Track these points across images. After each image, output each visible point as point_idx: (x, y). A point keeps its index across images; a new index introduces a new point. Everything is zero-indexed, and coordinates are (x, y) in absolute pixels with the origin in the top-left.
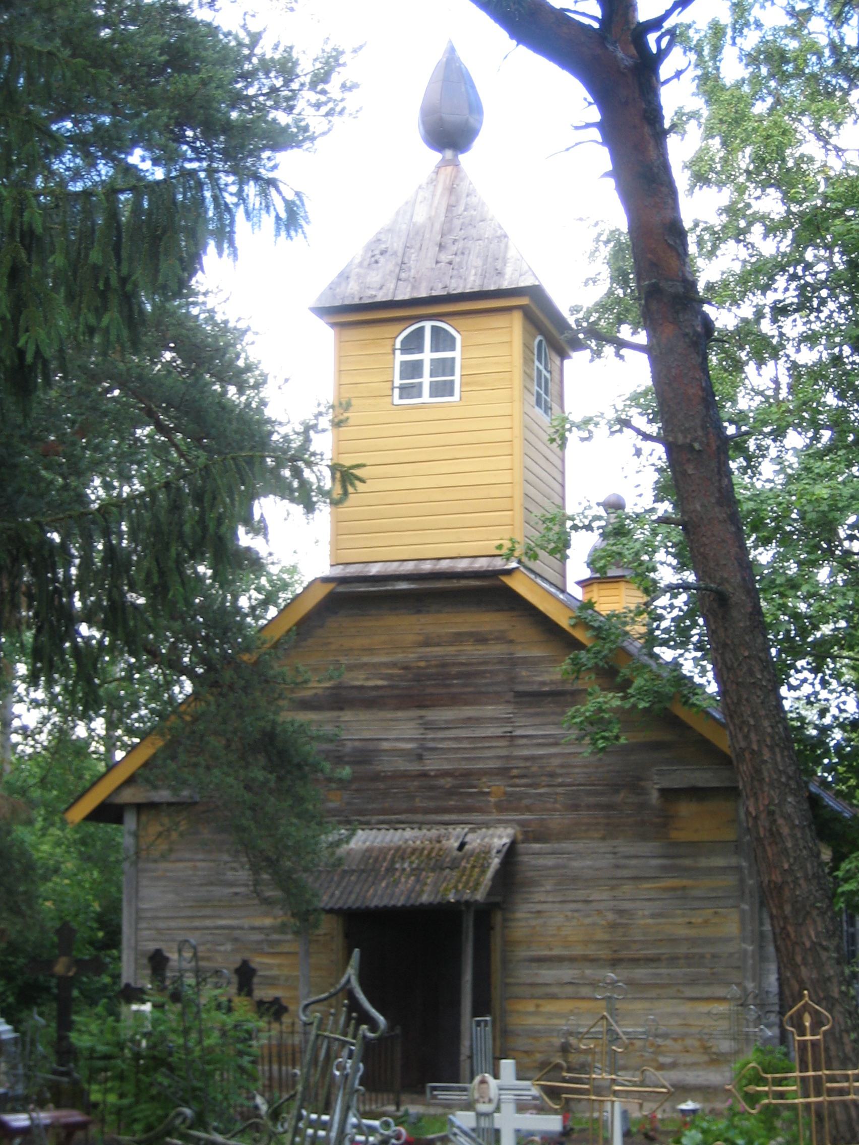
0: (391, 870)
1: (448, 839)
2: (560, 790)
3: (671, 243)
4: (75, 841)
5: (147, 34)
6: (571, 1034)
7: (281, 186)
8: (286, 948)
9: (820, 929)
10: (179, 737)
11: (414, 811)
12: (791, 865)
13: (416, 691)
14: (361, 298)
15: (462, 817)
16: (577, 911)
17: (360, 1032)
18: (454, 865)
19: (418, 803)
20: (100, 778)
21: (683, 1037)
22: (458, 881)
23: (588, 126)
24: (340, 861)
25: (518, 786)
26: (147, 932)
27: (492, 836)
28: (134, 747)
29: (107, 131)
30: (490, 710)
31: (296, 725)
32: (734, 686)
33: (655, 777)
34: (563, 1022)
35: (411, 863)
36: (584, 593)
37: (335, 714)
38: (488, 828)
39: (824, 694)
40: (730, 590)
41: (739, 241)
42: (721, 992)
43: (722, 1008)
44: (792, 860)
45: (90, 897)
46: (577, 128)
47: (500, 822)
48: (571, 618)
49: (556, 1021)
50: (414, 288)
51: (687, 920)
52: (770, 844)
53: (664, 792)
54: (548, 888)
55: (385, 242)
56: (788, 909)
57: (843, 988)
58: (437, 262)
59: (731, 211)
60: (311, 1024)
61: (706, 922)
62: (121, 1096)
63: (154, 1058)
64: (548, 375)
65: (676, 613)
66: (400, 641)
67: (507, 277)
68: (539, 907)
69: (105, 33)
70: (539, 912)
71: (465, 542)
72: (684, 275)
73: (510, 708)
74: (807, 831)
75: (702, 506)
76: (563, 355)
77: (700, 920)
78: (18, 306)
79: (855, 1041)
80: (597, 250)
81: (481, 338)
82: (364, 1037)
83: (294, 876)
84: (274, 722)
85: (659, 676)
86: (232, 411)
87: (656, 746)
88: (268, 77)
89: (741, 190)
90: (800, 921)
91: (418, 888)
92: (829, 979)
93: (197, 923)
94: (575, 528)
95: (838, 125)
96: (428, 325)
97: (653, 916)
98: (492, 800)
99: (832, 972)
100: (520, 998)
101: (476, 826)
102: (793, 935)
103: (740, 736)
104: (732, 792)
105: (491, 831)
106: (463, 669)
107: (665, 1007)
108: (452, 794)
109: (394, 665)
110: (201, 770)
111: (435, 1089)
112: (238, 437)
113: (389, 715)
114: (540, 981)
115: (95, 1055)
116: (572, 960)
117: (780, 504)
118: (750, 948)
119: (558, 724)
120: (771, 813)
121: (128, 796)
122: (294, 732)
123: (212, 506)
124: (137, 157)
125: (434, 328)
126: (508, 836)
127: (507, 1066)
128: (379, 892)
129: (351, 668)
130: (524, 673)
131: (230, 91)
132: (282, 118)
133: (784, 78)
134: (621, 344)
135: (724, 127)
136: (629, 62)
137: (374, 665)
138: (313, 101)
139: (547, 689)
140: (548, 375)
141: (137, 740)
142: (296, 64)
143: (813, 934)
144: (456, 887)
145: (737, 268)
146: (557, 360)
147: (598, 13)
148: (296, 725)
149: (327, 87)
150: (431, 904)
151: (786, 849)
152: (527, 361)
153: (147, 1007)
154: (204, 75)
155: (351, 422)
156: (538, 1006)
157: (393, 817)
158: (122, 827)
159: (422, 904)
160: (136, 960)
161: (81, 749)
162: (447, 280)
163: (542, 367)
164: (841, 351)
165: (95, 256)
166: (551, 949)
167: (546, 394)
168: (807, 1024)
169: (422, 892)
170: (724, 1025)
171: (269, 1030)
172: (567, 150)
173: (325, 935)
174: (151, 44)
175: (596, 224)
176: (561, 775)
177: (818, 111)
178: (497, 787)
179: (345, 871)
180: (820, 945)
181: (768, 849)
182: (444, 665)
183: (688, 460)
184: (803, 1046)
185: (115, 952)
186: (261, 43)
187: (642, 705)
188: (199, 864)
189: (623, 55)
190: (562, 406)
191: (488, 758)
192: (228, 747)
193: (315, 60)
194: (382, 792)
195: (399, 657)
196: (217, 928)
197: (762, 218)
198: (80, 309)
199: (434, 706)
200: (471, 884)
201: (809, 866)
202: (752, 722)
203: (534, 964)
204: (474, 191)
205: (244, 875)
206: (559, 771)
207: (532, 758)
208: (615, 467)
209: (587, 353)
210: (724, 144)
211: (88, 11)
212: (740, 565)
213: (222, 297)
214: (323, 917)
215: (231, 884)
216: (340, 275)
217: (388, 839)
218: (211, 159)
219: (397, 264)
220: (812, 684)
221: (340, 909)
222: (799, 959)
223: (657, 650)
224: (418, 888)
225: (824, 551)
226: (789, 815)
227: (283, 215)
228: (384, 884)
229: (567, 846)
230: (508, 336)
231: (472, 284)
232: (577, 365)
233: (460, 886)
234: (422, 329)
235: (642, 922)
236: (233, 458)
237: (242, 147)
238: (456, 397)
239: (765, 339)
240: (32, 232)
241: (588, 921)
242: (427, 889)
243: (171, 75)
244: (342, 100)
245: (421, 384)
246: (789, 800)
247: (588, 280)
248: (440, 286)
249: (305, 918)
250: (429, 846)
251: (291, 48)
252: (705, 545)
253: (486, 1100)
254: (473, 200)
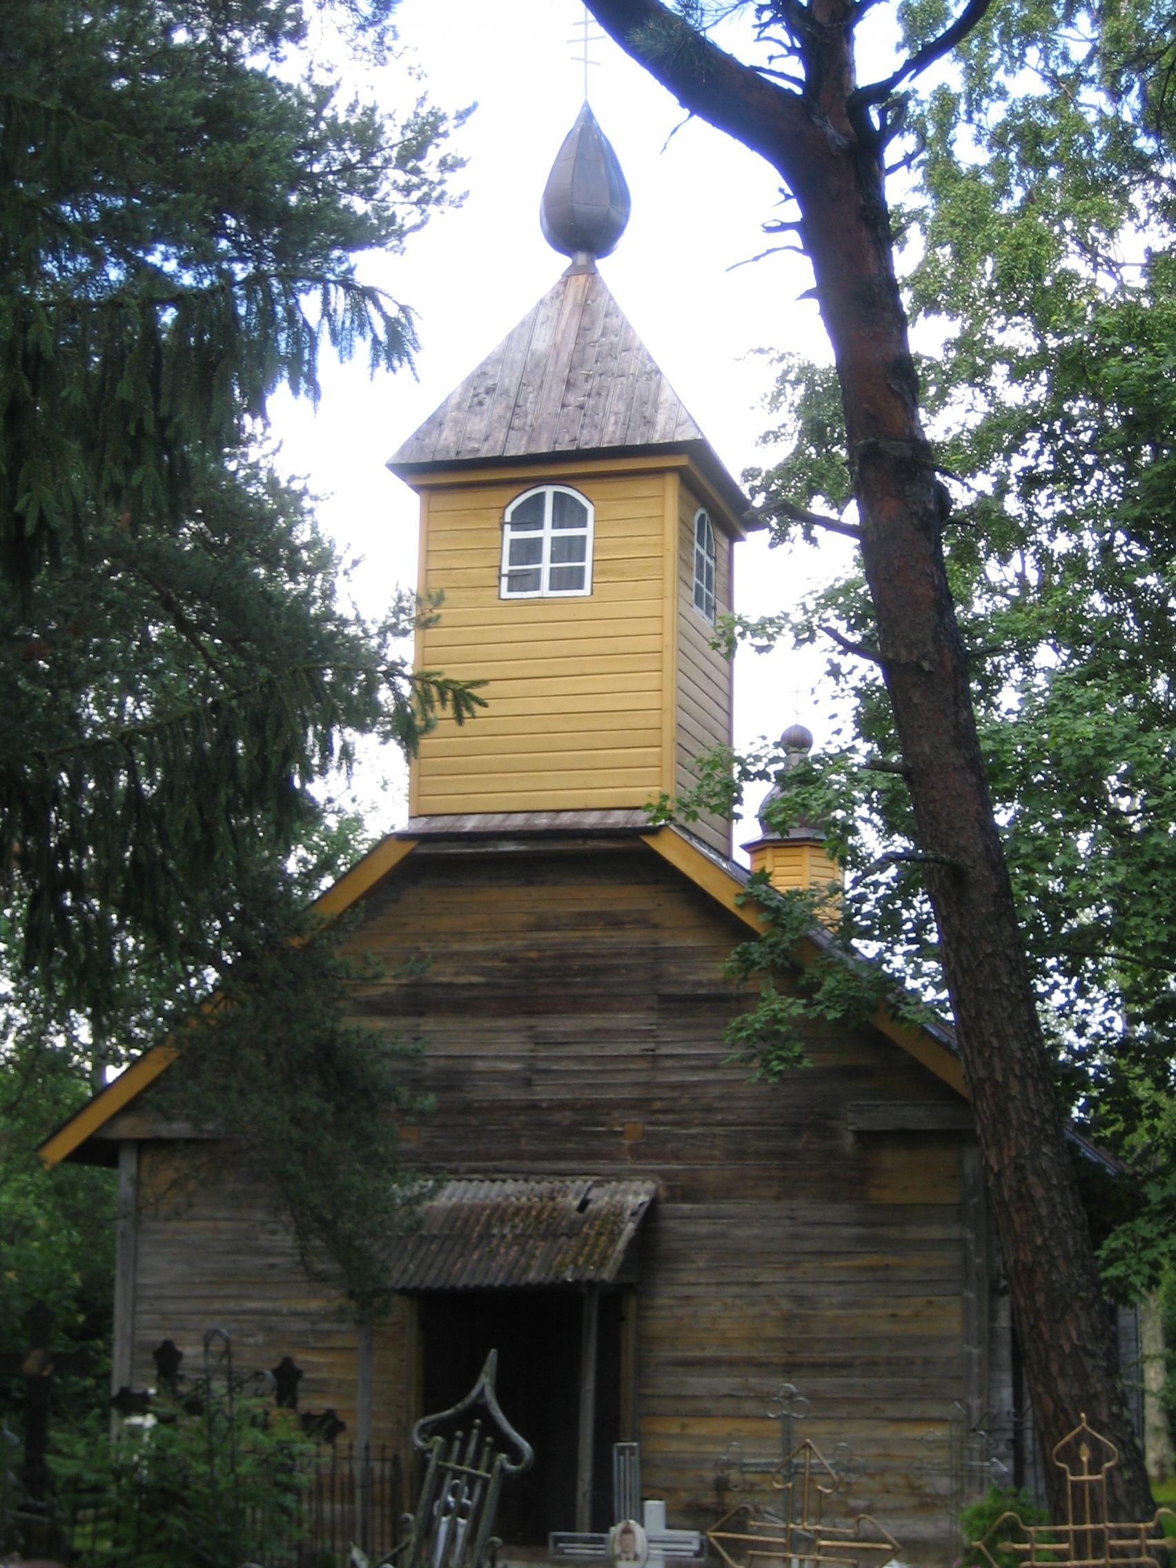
0: (486, 1236)
1: (565, 1195)
2: (718, 1130)
3: (896, 388)
4: (47, 1191)
5: (179, 88)
6: (729, 1465)
7: (383, 300)
8: (338, 1342)
9: (1083, 1328)
10: (198, 1053)
11: (518, 1156)
12: (1045, 1239)
13: (524, 991)
14: (458, 453)
15: (584, 1166)
16: (739, 1296)
17: (498, 1463)
18: (573, 1231)
19: (524, 1145)
20: (87, 1104)
21: (882, 1472)
22: (579, 1254)
23: (784, 227)
24: (420, 1222)
25: (662, 1124)
26: (147, 1317)
27: (625, 1192)
28: (135, 1061)
29: (121, 218)
30: (624, 1020)
31: (363, 1036)
32: (972, 995)
33: (850, 1115)
34: (720, 1449)
35: (514, 1227)
36: (753, 862)
37: (412, 1021)
38: (619, 1181)
39: (1081, 1005)
40: (969, 863)
41: (972, 384)
42: (937, 1411)
43: (939, 1432)
44: (1047, 1233)
45: (68, 1267)
46: (770, 230)
47: (636, 1173)
48: (738, 895)
49: (709, 1448)
50: (531, 440)
51: (890, 1311)
52: (1018, 1211)
53: (860, 1135)
54: (701, 1264)
55: (492, 377)
56: (1040, 1299)
57: (1115, 1409)
58: (563, 406)
59: (964, 344)
60: (430, 1451)
61: (916, 1314)
62: (117, 1543)
63: (163, 1491)
64: (712, 563)
65: (882, 891)
66: (502, 922)
67: (659, 427)
68: (689, 1291)
69: (121, 83)
70: (687, 1297)
71: (606, 786)
72: (911, 432)
73: (653, 1018)
74: (1069, 1194)
75: (933, 747)
76: (734, 536)
77: (907, 1312)
78: (17, 456)
79: (1130, 1481)
80: (780, 393)
81: (621, 510)
82: (503, 1470)
83: (357, 1243)
84: (333, 1031)
85: (856, 977)
86: (281, 604)
87: (848, 1073)
88: (340, 149)
89: (979, 319)
90: (1057, 1316)
91: (523, 1261)
92: (1095, 1396)
93: (216, 1306)
94: (745, 774)
95: (1111, 233)
96: (549, 491)
97: (844, 1305)
98: (626, 1142)
99: (1099, 1387)
100: (662, 1415)
101: (604, 1179)
102: (1046, 1336)
103: (979, 1062)
104: (958, 1137)
105: (623, 1186)
106: (589, 962)
107: (858, 1430)
108: (574, 1133)
109: (495, 955)
110: (234, 1096)
111: (559, 1540)
112: (289, 640)
113: (487, 1024)
114: (687, 1391)
115: (81, 1486)
116: (731, 1363)
117: (1029, 744)
118: (976, 1351)
119: (719, 1040)
120: (1020, 1168)
121: (126, 1129)
122: (360, 1045)
123: (277, 735)
124: (162, 258)
125: (557, 495)
126: (647, 1193)
127: (655, 1508)
128: (470, 1267)
129: (437, 958)
130: (673, 969)
131: (289, 167)
132: (360, 206)
133: (1041, 164)
134: (810, 521)
135: (957, 232)
136: (841, 142)
137: (466, 955)
138: (401, 183)
139: (703, 991)
140: (712, 563)
141: (138, 1053)
142: (379, 131)
143: (1074, 1334)
144: (574, 1262)
145: (975, 420)
146: (725, 543)
147: (800, 73)
148: (363, 1036)
149: (422, 165)
150: (540, 1284)
151: (1039, 1218)
152: (684, 543)
153: (149, 1421)
154: (252, 143)
155: (443, 621)
156: (684, 1426)
157: (490, 1164)
158: (116, 1171)
159: (527, 1285)
160: (132, 1354)
161: (59, 1062)
162: (576, 430)
163: (703, 552)
164: (1112, 538)
165: (124, 390)
166: (703, 1349)
167: (709, 588)
168: (1084, 1459)
169: (528, 1267)
170: (940, 1456)
171: (318, 1455)
172: (756, 259)
173: (394, 1324)
174: (183, 102)
175: (782, 358)
176: (720, 1110)
177: (1085, 211)
178: (633, 1125)
179: (423, 1238)
180: (1084, 1349)
181: (1015, 1216)
182: (563, 957)
183: (914, 685)
184: (1077, 1486)
185: (100, 1343)
186: (333, 102)
187: (831, 1015)
188: (222, 1224)
189: (835, 132)
190: (730, 606)
191: (624, 1085)
192: (268, 1063)
193: (405, 127)
194: (479, 1129)
195: (502, 944)
196: (244, 1312)
197: (1005, 355)
198: (102, 461)
199: (548, 1012)
200: (596, 1258)
201: (1070, 1241)
202: (995, 1043)
203: (680, 1369)
204: (616, 308)
205: (286, 1240)
206: (717, 1104)
207: (682, 1086)
208: (798, 690)
209: (764, 536)
210: (956, 254)
211: (97, 54)
212: (983, 829)
213: (268, 447)
214: (396, 1299)
215: (266, 1253)
216: (431, 420)
217: (482, 1194)
218: (260, 258)
219: (508, 407)
220: (1066, 992)
221: (416, 1289)
222: (1054, 1369)
223: (855, 942)
224: (523, 1261)
225: (1084, 809)
226: (1044, 1171)
227: (383, 337)
228: (475, 1257)
229: (727, 1207)
230: (658, 511)
231: (611, 435)
232: (752, 549)
233: (581, 1260)
234: (541, 496)
235: (829, 1313)
236: (307, 671)
237: (303, 243)
238: (586, 591)
239: (1009, 523)
240: (38, 355)
241: (754, 1311)
242: (536, 1263)
243: (208, 143)
244: (441, 182)
245: (538, 571)
246: (1045, 1150)
247: (767, 434)
248: (567, 437)
249: (366, 1298)
250: (539, 1205)
251: (373, 110)
252: (934, 801)
253: (631, 1556)
254: (615, 322)
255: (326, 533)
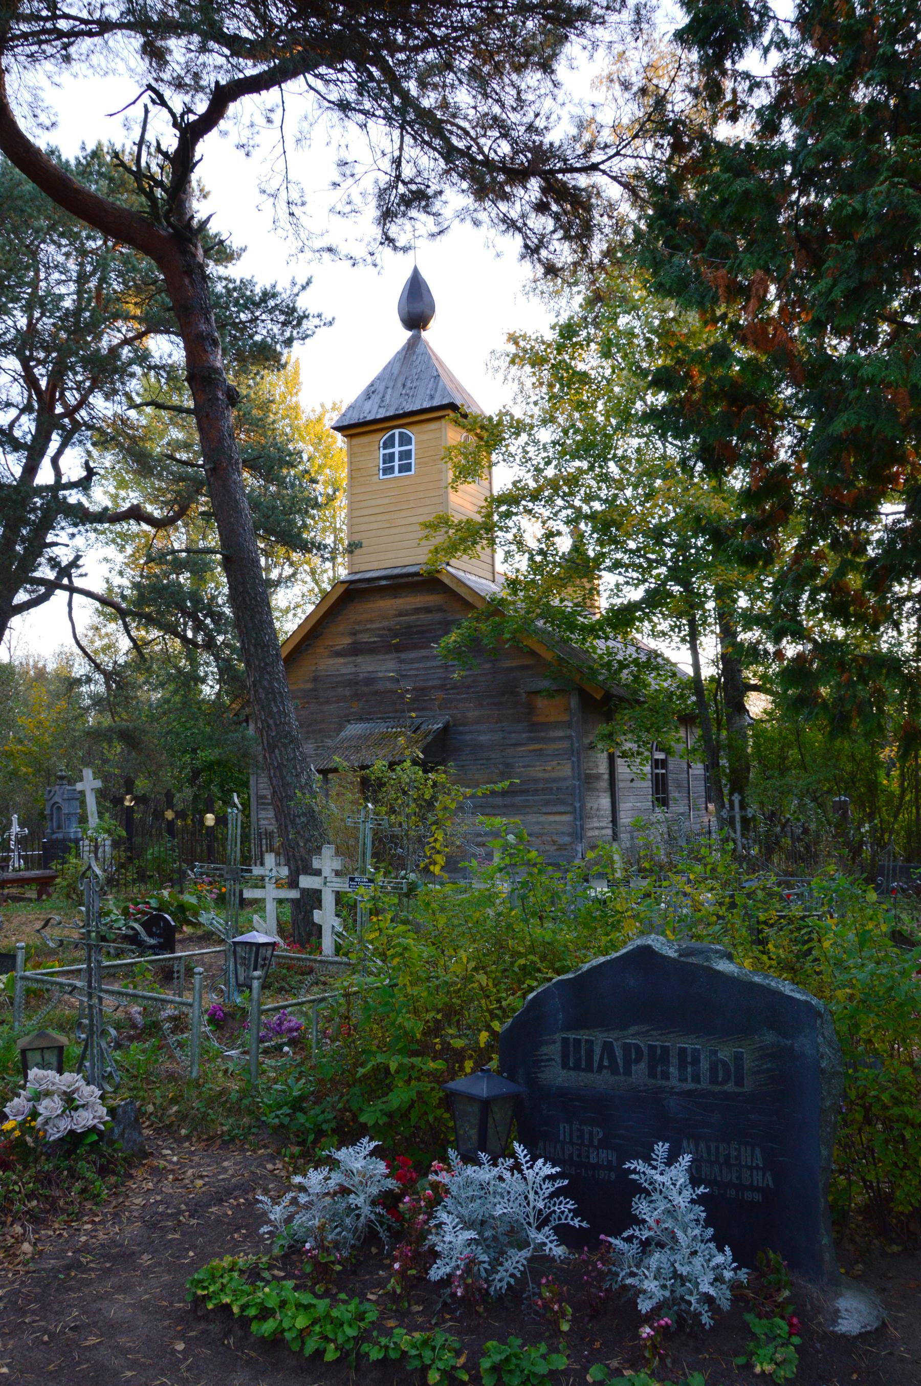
42: (562, 809)
81: (425, 437)
96: (397, 431)
113: (380, 657)
195: (385, 624)
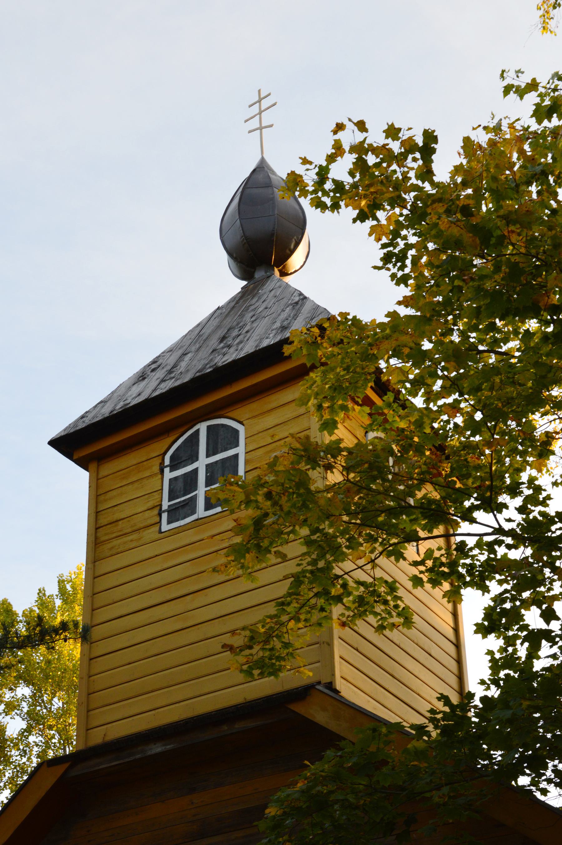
96: (203, 427)
255: (370, 321)
